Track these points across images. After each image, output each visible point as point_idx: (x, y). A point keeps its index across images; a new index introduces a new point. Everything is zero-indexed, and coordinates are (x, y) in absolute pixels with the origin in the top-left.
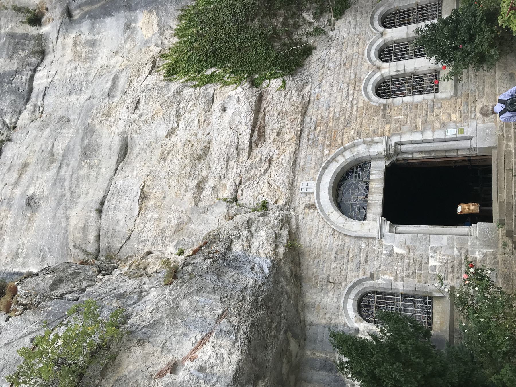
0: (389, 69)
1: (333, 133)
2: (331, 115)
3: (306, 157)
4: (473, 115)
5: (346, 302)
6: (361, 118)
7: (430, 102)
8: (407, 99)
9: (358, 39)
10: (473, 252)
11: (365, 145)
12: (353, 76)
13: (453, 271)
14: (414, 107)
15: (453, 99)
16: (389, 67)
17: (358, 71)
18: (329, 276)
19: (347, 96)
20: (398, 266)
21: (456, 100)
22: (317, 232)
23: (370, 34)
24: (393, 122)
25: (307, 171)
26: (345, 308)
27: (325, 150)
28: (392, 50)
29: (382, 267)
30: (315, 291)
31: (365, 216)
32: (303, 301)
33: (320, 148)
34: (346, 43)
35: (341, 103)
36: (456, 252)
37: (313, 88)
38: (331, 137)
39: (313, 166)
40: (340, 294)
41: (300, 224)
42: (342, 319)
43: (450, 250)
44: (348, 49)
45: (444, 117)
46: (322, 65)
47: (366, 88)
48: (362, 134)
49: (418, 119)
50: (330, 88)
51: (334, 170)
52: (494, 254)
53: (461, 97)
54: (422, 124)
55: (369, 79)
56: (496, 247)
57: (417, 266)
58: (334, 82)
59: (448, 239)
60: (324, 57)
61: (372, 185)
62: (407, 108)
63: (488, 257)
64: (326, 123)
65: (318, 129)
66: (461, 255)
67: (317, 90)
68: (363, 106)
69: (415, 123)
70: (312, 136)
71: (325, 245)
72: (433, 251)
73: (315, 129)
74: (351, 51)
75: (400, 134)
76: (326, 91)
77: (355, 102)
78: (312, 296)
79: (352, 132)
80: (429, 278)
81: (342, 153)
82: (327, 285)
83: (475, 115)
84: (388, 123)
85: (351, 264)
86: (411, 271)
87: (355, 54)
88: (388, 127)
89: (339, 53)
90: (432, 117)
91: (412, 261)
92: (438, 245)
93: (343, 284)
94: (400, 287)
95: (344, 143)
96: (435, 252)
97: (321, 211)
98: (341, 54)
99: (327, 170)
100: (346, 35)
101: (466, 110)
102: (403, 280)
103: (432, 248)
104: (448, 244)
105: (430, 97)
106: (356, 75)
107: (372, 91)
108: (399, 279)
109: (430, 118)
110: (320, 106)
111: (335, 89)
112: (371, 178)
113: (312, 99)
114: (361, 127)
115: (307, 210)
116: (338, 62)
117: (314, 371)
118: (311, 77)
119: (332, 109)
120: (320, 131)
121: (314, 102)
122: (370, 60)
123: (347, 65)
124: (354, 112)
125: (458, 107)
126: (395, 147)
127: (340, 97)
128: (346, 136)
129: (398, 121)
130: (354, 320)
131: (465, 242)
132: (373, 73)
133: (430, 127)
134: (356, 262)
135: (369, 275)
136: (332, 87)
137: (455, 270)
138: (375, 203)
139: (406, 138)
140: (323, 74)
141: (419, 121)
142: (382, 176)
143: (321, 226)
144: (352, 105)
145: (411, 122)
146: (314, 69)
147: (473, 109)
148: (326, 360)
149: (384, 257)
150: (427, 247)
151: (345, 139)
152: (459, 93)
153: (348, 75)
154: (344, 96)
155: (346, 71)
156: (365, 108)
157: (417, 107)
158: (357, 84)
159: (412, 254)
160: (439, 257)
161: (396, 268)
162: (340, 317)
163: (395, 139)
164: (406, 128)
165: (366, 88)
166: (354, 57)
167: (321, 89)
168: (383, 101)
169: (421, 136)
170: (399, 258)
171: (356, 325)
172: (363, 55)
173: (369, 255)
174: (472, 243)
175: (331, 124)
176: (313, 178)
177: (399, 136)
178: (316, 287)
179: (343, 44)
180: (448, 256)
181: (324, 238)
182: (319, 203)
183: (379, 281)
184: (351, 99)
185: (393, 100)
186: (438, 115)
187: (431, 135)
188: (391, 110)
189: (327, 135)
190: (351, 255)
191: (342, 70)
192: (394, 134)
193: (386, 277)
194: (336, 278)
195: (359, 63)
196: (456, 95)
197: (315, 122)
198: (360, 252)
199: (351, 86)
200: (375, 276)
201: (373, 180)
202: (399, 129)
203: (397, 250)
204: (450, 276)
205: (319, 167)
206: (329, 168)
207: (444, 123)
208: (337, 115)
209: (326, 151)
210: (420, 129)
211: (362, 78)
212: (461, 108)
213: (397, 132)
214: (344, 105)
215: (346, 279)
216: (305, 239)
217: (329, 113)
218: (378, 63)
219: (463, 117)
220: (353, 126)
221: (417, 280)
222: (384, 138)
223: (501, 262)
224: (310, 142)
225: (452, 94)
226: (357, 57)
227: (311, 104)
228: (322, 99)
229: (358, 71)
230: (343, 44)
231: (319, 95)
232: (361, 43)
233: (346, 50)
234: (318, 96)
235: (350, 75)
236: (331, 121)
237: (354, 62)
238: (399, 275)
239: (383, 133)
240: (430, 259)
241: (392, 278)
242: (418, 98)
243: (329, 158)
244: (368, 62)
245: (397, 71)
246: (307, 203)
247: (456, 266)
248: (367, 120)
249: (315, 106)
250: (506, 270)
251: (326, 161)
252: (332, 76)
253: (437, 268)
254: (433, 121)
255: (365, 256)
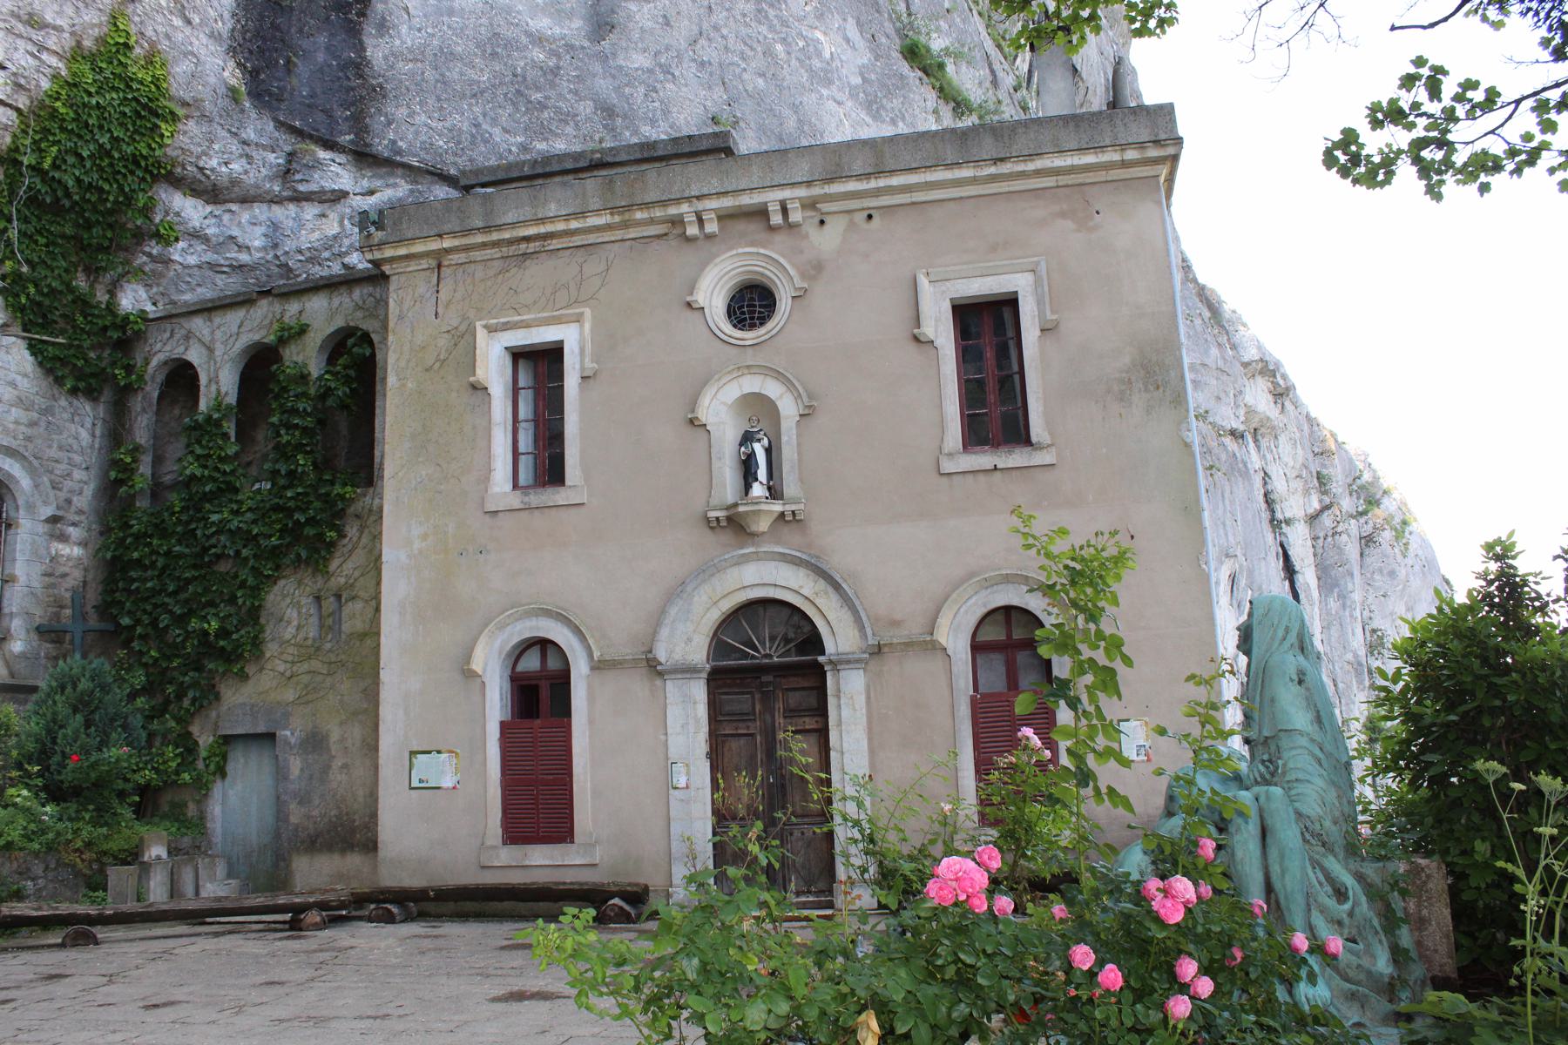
182: (1535, 94)
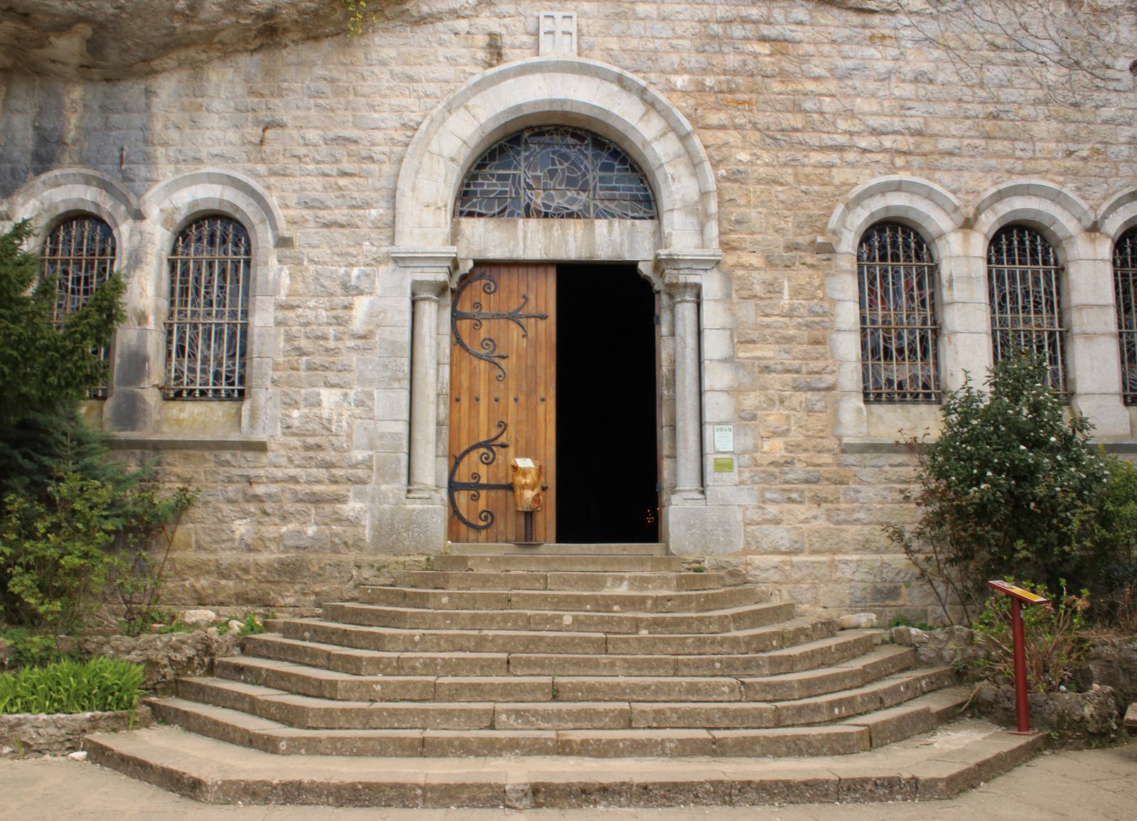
0: (963, 260)
1: (746, 97)
2: (811, 86)
3: (664, 19)
4: (774, 496)
5: (212, 178)
6: (790, 179)
7: (829, 379)
8: (848, 313)
9: (1085, 153)
10: (360, 496)
11: (696, 198)
12: (945, 144)
13: (308, 448)
14: (818, 333)
15: (831, 443)
16: (967, 257)
17: (964, 162)
18: (282, 125)
19: (874, 132)
20: (316, 310)
21: (829, 451)
22: (411, 79)
23: (1099, 191)
24: (769, 276)
25: (618, 28)
26: (195, 180)
27: (686, 77)
28: (1035, 262)
29: (312, 267)
30: (239, 91)
31: (480, 215)
32: (210, 60)
33: (694, 60)
34: (1079, 116)
35: (851, 114)
36: (359, 455)
37: (915, 19)
38: (731, 91)
39: (634, 43)
40: (234, 161)
41: (439, 25)
42: (166, 173)
43: (365, 441)
44: (1054, 125)
45: (774, 418)
46: (999, 41)
47: (898, 187)
48: (736, 186)
49: (777, 347)
50: (910, 76)
51: (615, 111)
52: (358, 544)
53: (839, 465)
54: (758, 358)
55: (930, 195)
56: (377, 550)
57: (317, 360)
58: (930, 87)
59: (394, 436)
60: (1030, 46)
61: (574, 229)
62: (817, 314)
63: (350, 530)
64: (782, 72)
65: (765, 49)
66: (354, 466)
67: (907, 32)
68: (836, 181)
69: (764, 340)
70: (737, 31)
71: (372, 107)
72: (362, 397)
73: (763, 39)
74: (1044, 134)
75: (729, 296)
76: (902, 63)
77: (851, 156)
78: (225, 82)
79: (744, 156)
80: (287, 389)
81: (673, 130)
82: (257, 123)
83: (774, 501)
84: (770, 262)
85: (318, 183)
86: (303, 343)
87: (1029, 146)
88: (755, 260)
89: (1040, 94)
90: (777, 386)
91: (331, 344)
92: (378, 412)
93: (261, 168)
94: (262, 319)
95: (709, 133)
96: (360, 403)
97: (477, 84)
98: (1036, 102)
99: (615, 88)
100: (1107, 113)
101: (791, 476)
102: (278, 323)
103: (370, 396)
104: (382, 436)
105: (850, 375)
106: (951, 154)
107: (887, 208)
108: (280, 315)
109: (774, 380)
110: (846, 48)
111: (907, 90)
112: (598, 222)
113: (876, 19)
114: (759, 181)
115: (482, 40)
116: (1004, 94)
117: (32, 113)
118: (958, 10)
119: (832, 86)
120: (756, 55)
121: (864, 27)
122: (1000, 196)
123: (989, 125)
124: (816, 157)
125: (803, 456)
126: (686, 286)
127: (875, 108)
128: (733, 137)
129: (773, 289)
130: (166, 204)
131: (387, 474)
132: (949, 208)
133: (746, 381)
134: (323, 196)
135: (286, 234)
136: (916, 80)
137: (311, 454)
138: (515, 238)
139: (713, 315)
140: (968, 48)
141: (767, 351)
142: (604, 253)
143: (432, 88)
144: (840, 149)
145: (768, 326)
146: (990, 16)
147: (794, 496)
148: (61, 142)
149: (342, 270)
150: (371, 382)
151: (720, 134)
152: (851, 459)
153: (953, 128)
154: (875, 122)
155: (968, 123)
156: (829, 189)
157: (816, 342)
158: (916, 161)
159: (352, 343)
160: (346, 414)
161: (312, 303)
162: (172, 167)
163: (711, 285)
164: (748, 312)
165: (898, 187)
166: (1020, 145)
167: (909, 44)
168: (848, 243)
169: (718, 356)
170: (340, 312)
171: (153, 213)
172: (1024, 173)
173: (346, 231)
174: (385, 495)
175: (776, 86)
176: (591, 48)
177: (719, 295)
178: (252, 93)
179: (1075, 105)
180: (349, 436)
181: (394, 101)
182: (504, 76)
183: (273, 261)
184: (863, 144)
185: (847, 272)
186: (782, 401)
187: (718, 386)
188: (812, 266)
189: (739, 80)
190: (343, 182)
191: (976, 109)
192: (728, 278)
193: (286, 281)
194: (278, 147)
195: (993, 162)
196: (844, 451)
197: (789, 35)
198: (352, 207)
199: (911, 140)
200: (287, 252)
201: (592, 230)
202: (745, 293)
203: (362, 305)
204: (295, 442)
205: (628, 63)
206: (624, 94)
207: (754, 418)
208: (809, 105)
209: (681, 81)
210: (741, 355)
211: (938, 175)
212: (798, 465)
213: (735, 289)
214: (842, 125)
215: (275, 174)
216: (390, 45)
217: (817, 79)
218: (989, 222)
219: (772, 469)
220: (766, 157)
221: (281, 359)
222: (714, 250)
223: (335, 558)
224: (717, 29)
225: (845, 440)
226: (1019, 153)
227: (855, 19)
228: (871, 51)
229: (964, 162)
230: (1075, 105)
231: (888, 42)
232: (1069, 163)
233: (1047, 118)
234: (883, 37)
235: (951, 134)
236: (790, 87)
237: (999, 146)
238: (291, 314)
239: (734, 249)
240: (337, 391)
241: (282, 297)
242: (848, 347)
243: (653, 90)
244: (993, 190)
245: (951, 282)
246: (507, 40)
247: (320, 455)
248: (782, 197)
249: (847, 32)
250: (316, 569)
251: (643, 83)
252: (955, 79)
253: (316, 410)
254: (764, 388)
255: (342, 220)
